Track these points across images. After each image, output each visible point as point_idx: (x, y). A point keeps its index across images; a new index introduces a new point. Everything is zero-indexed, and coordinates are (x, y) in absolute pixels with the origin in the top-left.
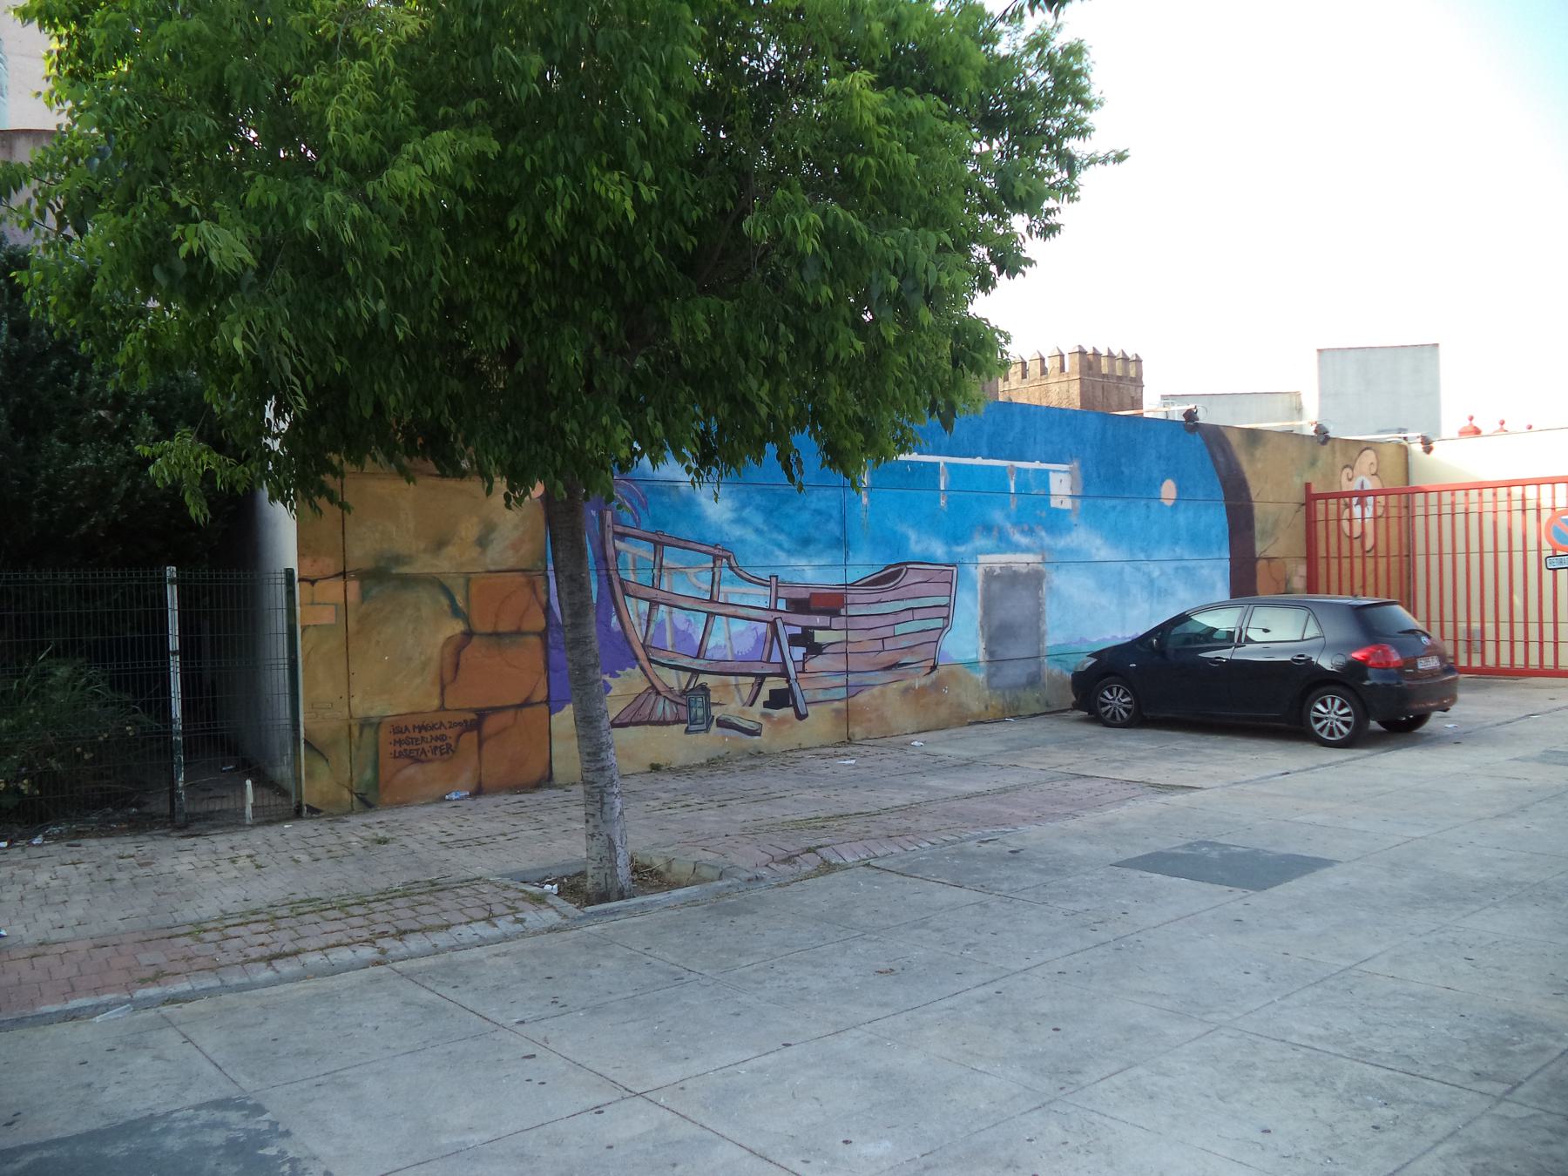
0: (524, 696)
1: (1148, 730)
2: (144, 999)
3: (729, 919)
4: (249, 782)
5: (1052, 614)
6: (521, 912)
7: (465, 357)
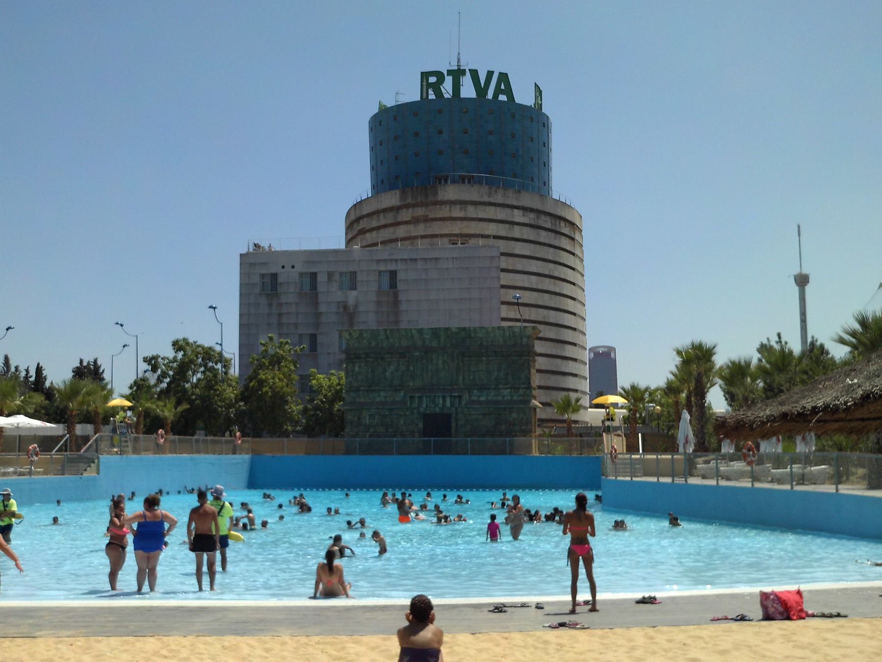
0: (8, 332)
2: (850, 551)
3: (442, 493)
5: (398, 196)
6: (781, 635)
7: (797, 451)
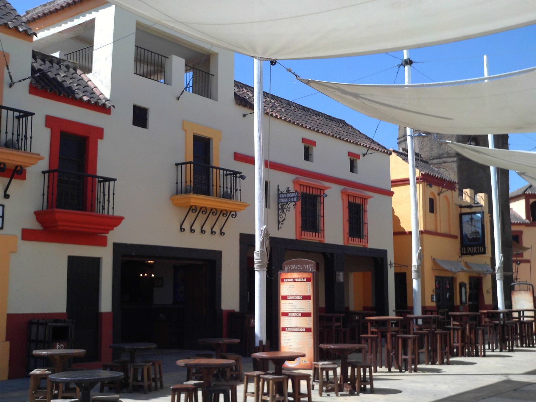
1: (459, 220)
4: (485, 57)
